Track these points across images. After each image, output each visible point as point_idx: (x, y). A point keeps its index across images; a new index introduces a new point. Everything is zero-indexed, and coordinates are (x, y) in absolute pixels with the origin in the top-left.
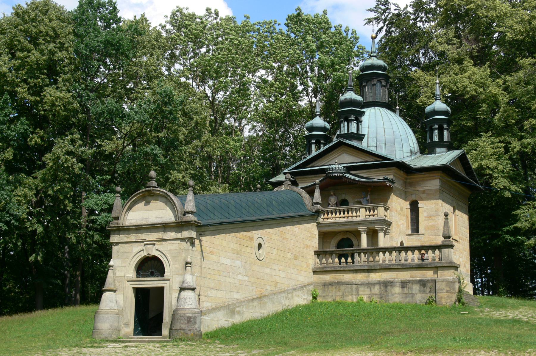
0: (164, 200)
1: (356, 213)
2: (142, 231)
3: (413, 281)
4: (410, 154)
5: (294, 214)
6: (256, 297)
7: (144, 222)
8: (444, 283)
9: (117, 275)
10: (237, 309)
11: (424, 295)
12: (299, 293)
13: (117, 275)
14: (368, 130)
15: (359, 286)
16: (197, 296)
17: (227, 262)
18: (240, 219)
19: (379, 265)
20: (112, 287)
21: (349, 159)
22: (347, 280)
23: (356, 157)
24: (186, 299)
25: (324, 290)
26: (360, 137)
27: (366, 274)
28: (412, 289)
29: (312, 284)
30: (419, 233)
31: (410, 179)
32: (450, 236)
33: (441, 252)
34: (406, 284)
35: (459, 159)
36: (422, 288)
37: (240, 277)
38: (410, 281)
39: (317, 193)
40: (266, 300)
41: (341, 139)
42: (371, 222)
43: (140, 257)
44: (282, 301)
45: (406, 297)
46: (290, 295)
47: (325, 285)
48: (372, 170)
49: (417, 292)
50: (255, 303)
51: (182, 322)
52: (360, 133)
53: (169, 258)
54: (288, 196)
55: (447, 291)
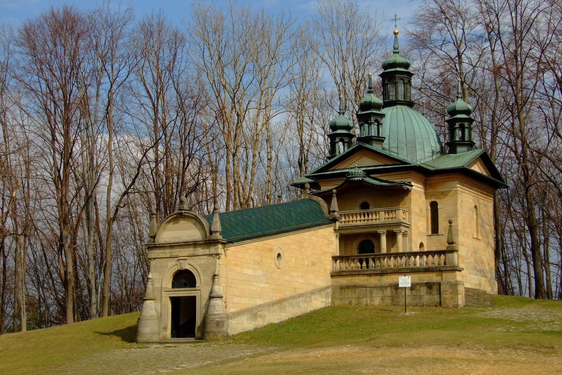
0: (194, 221)
1: (376, 216)
2: (175, 248)
4: (431, 154)
5: (311, 223)
7: (177, 241)
8: (447, 286)
9: (155, 286)
10: (259, 313)
12: (317, 296)
13: (155, 286)
15: (373, 288)
16: (223, 303)
17: (250, 272)
18: (260, 233)
19: (391, 269)
20: (151, 297)
21: (368, 162)
23: (375, 160)
24: (215, 306)
25: (341, 293)
26: (381, 140)
27: (378, 278)
28: (419, 291)
29: (330, 288)
30: (439, 234)
32: (454, 241)
33: (445, 256)
34: (415, 287)
36: (429, 290)
37: (262, 285)
39: (334, 201)
40: (285, 304)
42: (390, 225)
43: (175, 271)
44: (301, 304)
45: (415, 299)
46: (308, 299)
47: (342, 288)
48: (391, 174)
49: (424, 293)
50: (276, 307)
51: (212, 325)
52: (380, 136)
53: (200, 271)
55: (451, 293)
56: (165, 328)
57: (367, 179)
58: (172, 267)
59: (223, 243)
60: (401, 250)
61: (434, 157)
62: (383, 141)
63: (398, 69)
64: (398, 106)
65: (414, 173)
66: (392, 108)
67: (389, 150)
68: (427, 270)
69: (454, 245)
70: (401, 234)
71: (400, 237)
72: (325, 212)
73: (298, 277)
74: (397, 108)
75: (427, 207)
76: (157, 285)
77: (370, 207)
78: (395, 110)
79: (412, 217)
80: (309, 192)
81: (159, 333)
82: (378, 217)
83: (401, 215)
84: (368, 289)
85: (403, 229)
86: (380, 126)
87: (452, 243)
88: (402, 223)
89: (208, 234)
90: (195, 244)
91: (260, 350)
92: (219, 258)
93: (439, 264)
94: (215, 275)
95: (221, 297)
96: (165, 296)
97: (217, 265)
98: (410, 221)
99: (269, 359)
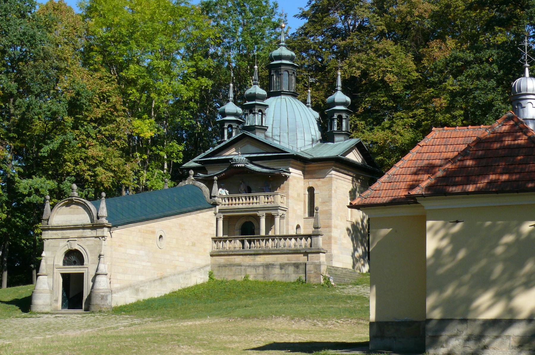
3: (289, 263)
4: (311, 143)
6: (157, 278)
8: (312, 266)
9: (48, 264)
10: (141, 288)
11: (297, 275)
12: (196, 273)
14: (273, 120)
15: (247, 267)
16: (108, 280)
17: (133, 252)
22: (238, 263)
26: (264, 129)
31: (308, 167)
35: (308, 176)
37: (144, 264)
38: (286, 264)
40: (165, 280)
41: (245, 132)
45: (283, 277)
49: (292, 272)
50: (157, 283)
53: (87, 251)
54: (190, 191)
56: (56, 301)
57: (250, 166)
58: (63, 247)
59: (109, 227)
60: (278, 233)
61: (314, 146)
62: (266, 130)
63: (284, 62)
64: (283, 97)
65: (292, 161)
66: (277, 97)
67: (272, 137)
68: (296, 252)
69: (319, 230)
70: (279, 216)
71: (277, 220)
72: (206, 197)
73: (178, 256)
74: (281, 98)
75: (304, 192)
76: (50, 263)
77: (252, 191)
78: (279, 100)
79: (290, 201)
80: (193, 178)
81: (51, 305)
82: (258, 201)
83: (278, 199)
84: (243, 268)
85: (280, 212)
86: (264, 116)
87: (318, 228)
88: (279, 207)
89: (95, 219)
90: (84, 227)
91: (136, 321)
92: (105, 240)
93: (306, 246)
94: (100, 255)
95: (106, 275)
96: (57, 273)
97: (103, 247)
98: (287, 205)
99: (185, 324)
